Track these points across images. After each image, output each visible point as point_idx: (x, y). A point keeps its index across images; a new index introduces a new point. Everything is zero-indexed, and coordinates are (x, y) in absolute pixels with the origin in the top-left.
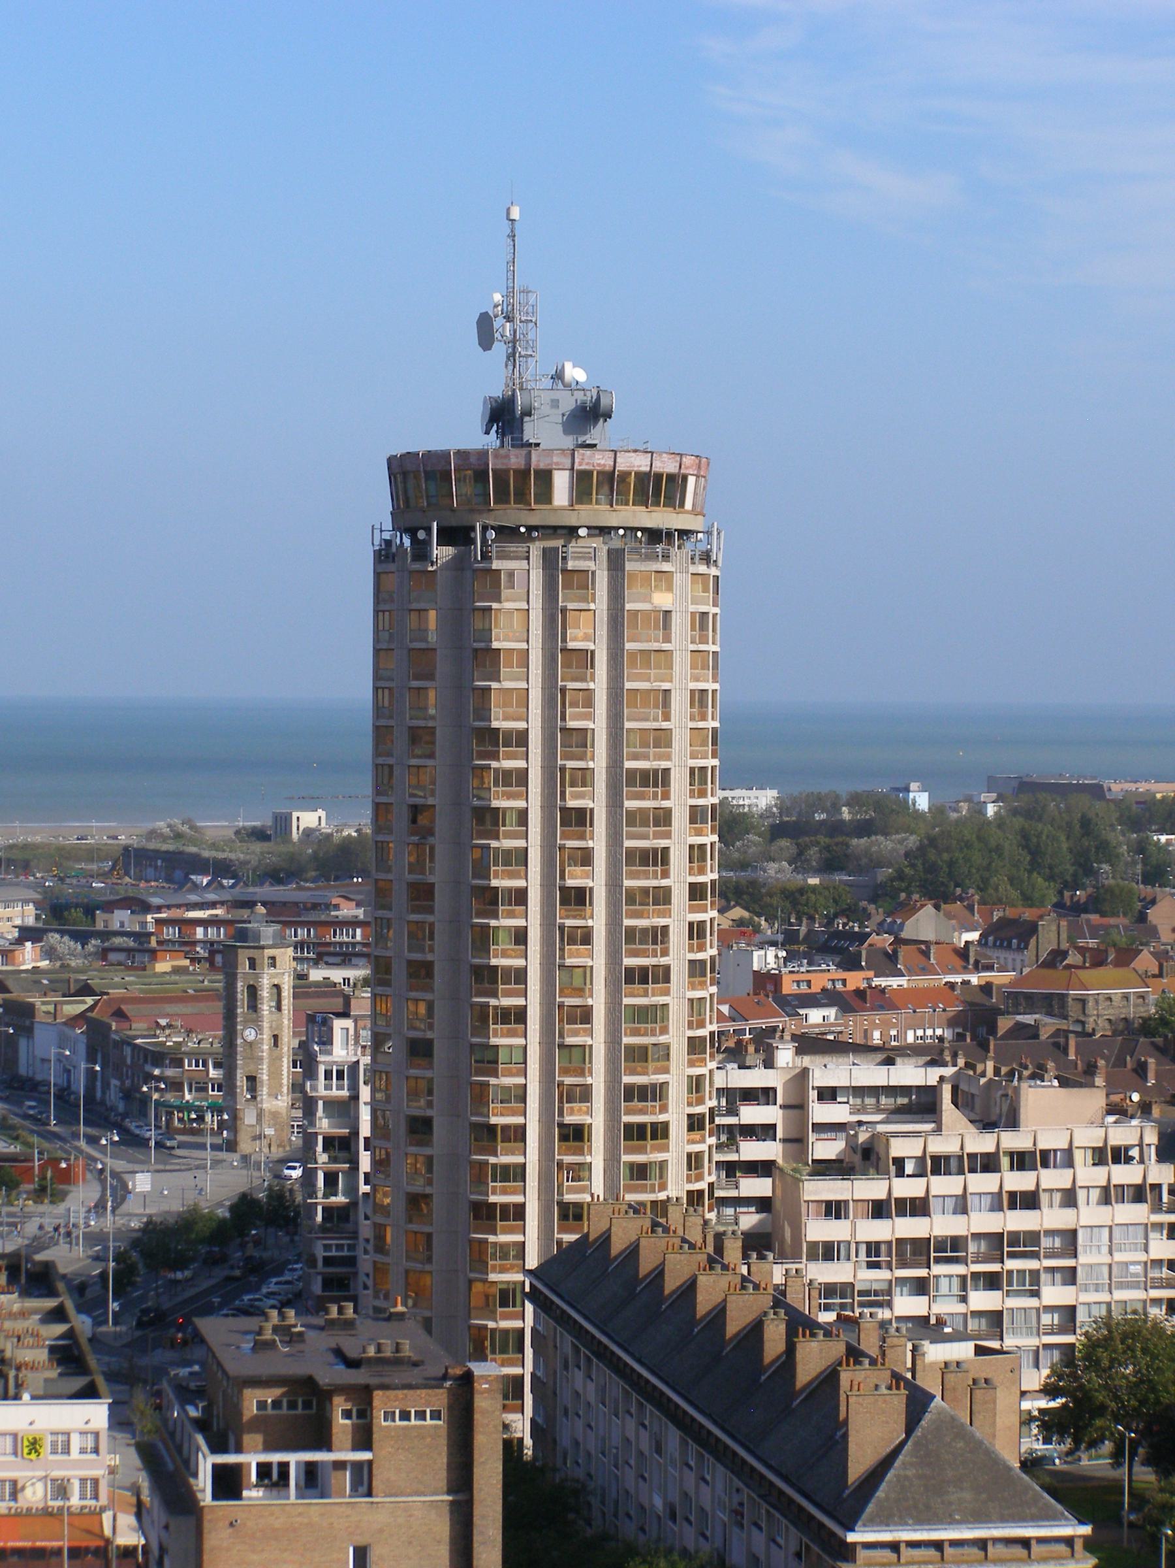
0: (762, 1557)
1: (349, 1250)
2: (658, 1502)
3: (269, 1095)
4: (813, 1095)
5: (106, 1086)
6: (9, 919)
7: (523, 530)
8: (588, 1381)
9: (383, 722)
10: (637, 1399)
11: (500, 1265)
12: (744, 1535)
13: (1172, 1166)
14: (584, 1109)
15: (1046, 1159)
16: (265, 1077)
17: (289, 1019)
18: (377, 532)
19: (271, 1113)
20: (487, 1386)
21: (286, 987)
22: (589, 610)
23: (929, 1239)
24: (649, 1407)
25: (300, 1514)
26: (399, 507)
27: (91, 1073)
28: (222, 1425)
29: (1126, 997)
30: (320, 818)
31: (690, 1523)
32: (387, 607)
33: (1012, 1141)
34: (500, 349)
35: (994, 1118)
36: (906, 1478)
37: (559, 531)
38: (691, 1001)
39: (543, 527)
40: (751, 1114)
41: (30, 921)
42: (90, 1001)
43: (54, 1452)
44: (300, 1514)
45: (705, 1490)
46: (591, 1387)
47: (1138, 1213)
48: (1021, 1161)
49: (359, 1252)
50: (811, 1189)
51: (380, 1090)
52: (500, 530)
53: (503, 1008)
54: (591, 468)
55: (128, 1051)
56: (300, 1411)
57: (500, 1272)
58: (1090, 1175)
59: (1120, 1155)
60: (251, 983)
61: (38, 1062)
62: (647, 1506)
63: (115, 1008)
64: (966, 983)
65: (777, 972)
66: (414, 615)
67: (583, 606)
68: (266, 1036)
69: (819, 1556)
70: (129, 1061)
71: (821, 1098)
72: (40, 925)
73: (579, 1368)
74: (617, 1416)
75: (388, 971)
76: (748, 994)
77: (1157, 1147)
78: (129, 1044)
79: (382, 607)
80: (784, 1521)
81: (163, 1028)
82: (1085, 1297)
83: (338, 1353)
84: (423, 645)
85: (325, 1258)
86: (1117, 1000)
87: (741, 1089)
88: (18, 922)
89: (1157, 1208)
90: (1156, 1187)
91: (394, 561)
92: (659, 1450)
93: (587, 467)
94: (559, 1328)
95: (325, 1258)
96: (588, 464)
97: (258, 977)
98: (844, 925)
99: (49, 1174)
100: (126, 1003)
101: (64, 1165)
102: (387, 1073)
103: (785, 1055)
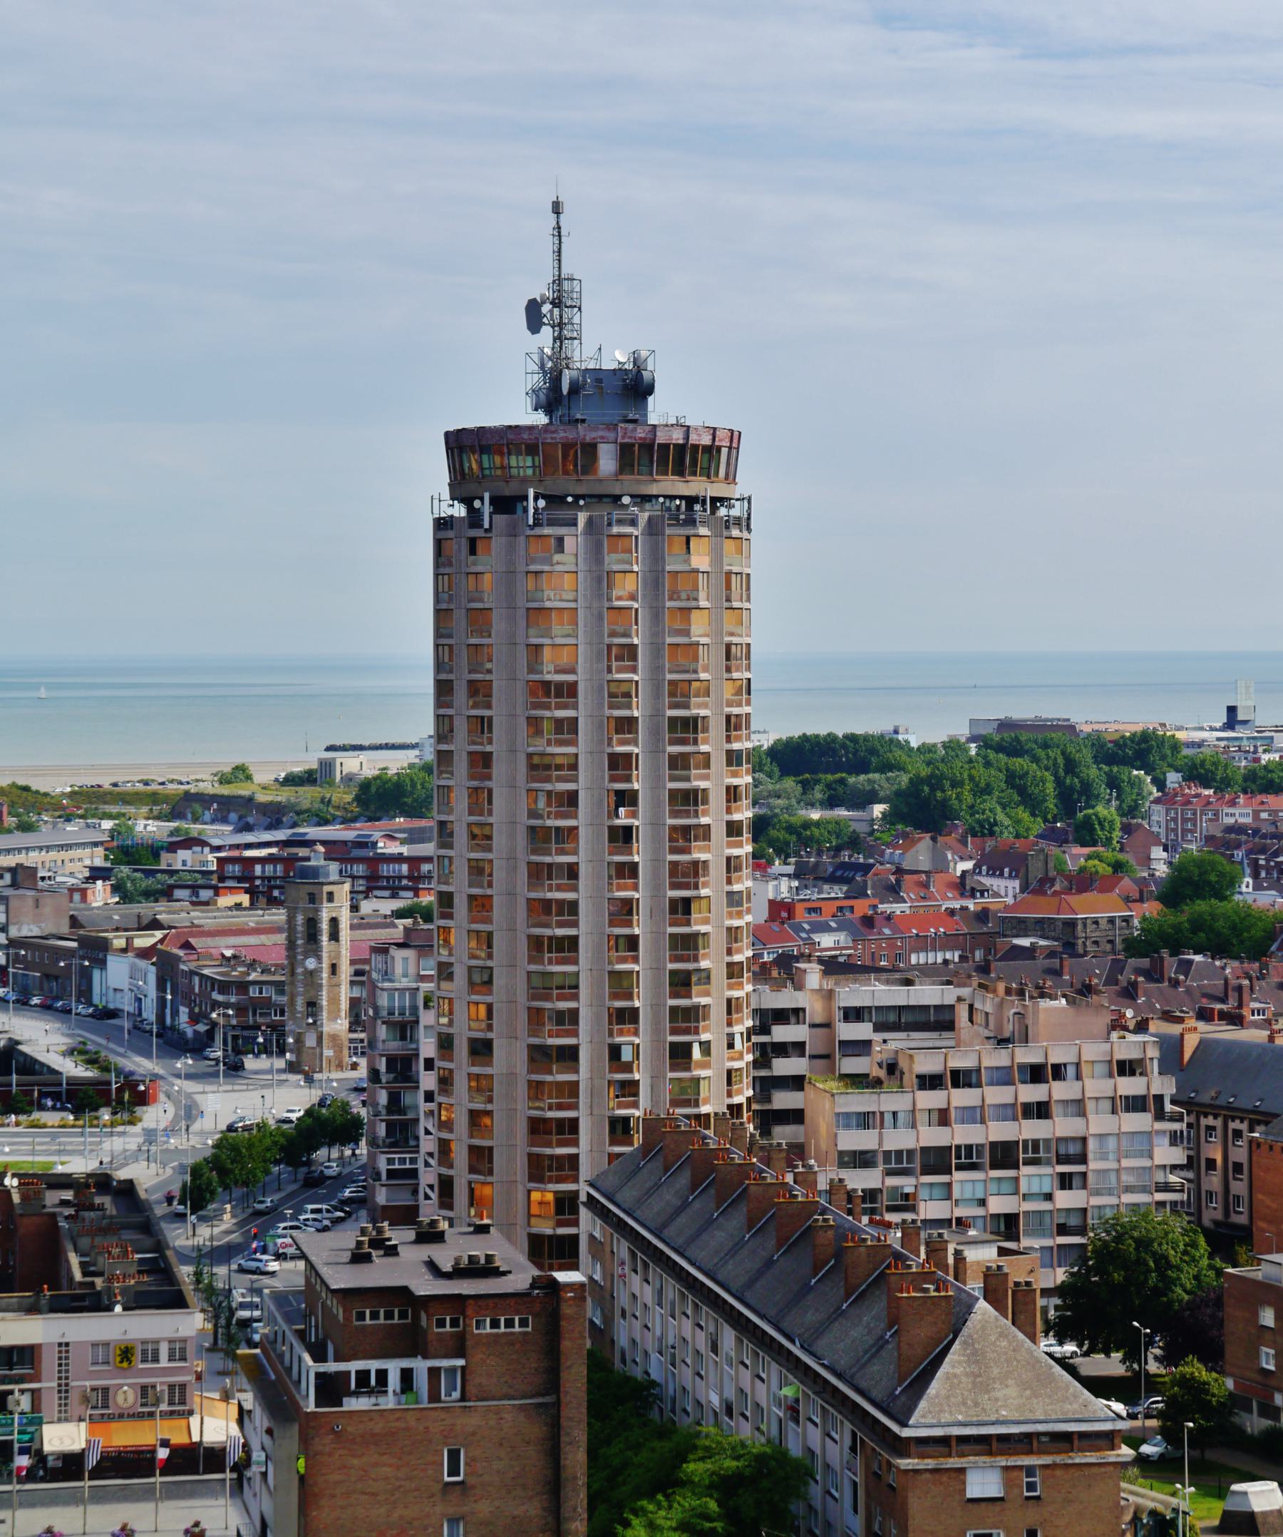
0: (818, 1451)
2: (715, 1399)
3: (329, 1020)
4: (838, 1015)
5: (175, 1013)
6: (80, 860)
7: (570, 499)
8: (645, 1284)
9: (443, 676)
12: (800, 1430)
13: (1174, 1080)
15: (1058, 1072)
16: (324, 1003)
18: (436, 502)
19: (330, 1036)
24: (704, 1308)
25: (398, 1419)
27: (162, 1002)
28: (321, 1336)
29: (1111, 921)
31: (746, 1418)
32: (447, 570)
33: (1027, 1055)
34: (547, 333)
35: (1007, 1034)
36: (955, 1375)
40: (781, 1033)
41: (99, 862)
42: (159, 934)
43: (144, 1361)
44: (398, 1419)
45: (761, 1389)
46: (648, 1290)
47: (1140, 1121)
48: (1036, 1074)
51: (444, 1015)
55: (196, 980)
56: (396, 1321)
58: (1097, 1086)
59: (1127, 1068)
61: (111, 993)
62: (703, 1402)
63: (183, 941)
64: (964, 909)
66: (471, 578)
67: (627, 567)
68: (325, 965)
69: (874, 1450)
70: (197, 990)
72: (108, 865)
73: (636, 1272)
74: (673, 1317)
75: (450, 905)
77: (1159, 1060)
78: (197, 974)
79: (442, 570)
80: (839, 1417)
82: (1095, 1201)
85: (388, 1170)
86: (1104, 924)
87: (773, 1010)
88: (88, 862)
89: (1160, 1115)
90: (1159, 1099)
92: (715, 1348)
94: (616, 1235)
97: (317, 910)
98: (850, 856)
99: (126, 1096)
100: (193, 936)
101: (142, 1088)
102: (451, 1000)
103: (813, 976)
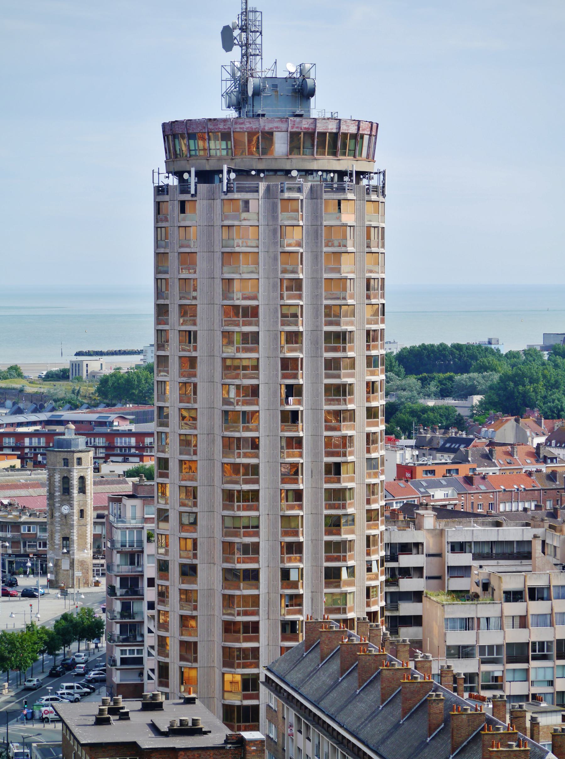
1: (138, 653)
4: (448, 548)
7: (253, 173)
10: (341, 752)
11: (243, 663)
14: (298, 558)
16: (75, 538)
17: (91, 499)
19: (79, 561)
20: (255, 748)
21: (89, 478)
22: (299, 226)
23: (528, 643)
26: (170, 157)
30: (102, 364)
34: (237, 51)
37: (279, 173)
38: (368, 485)
39: (268, 170)
40: (405, 561)
49: (145, 655)
50: (449, 610)
52: (239, 172)
53: (244, 491)
54: (300, 130)
57: (243, 668)
60: (65, 475)
65: (412, 465)
68: (76, 511)
71: (453, 550)
75: (167, 468)
76: (395, 480)
79: (160, 224)
81: (6, 506)
83: (154, 727)
84: (188, 250)
85: (121, 659)
91: (167, 194)
93: (297, 130)
94: (286, 705)
95: (121, 659)
96: (297, 128)
97: (70, 471)
98: (456, 433)
